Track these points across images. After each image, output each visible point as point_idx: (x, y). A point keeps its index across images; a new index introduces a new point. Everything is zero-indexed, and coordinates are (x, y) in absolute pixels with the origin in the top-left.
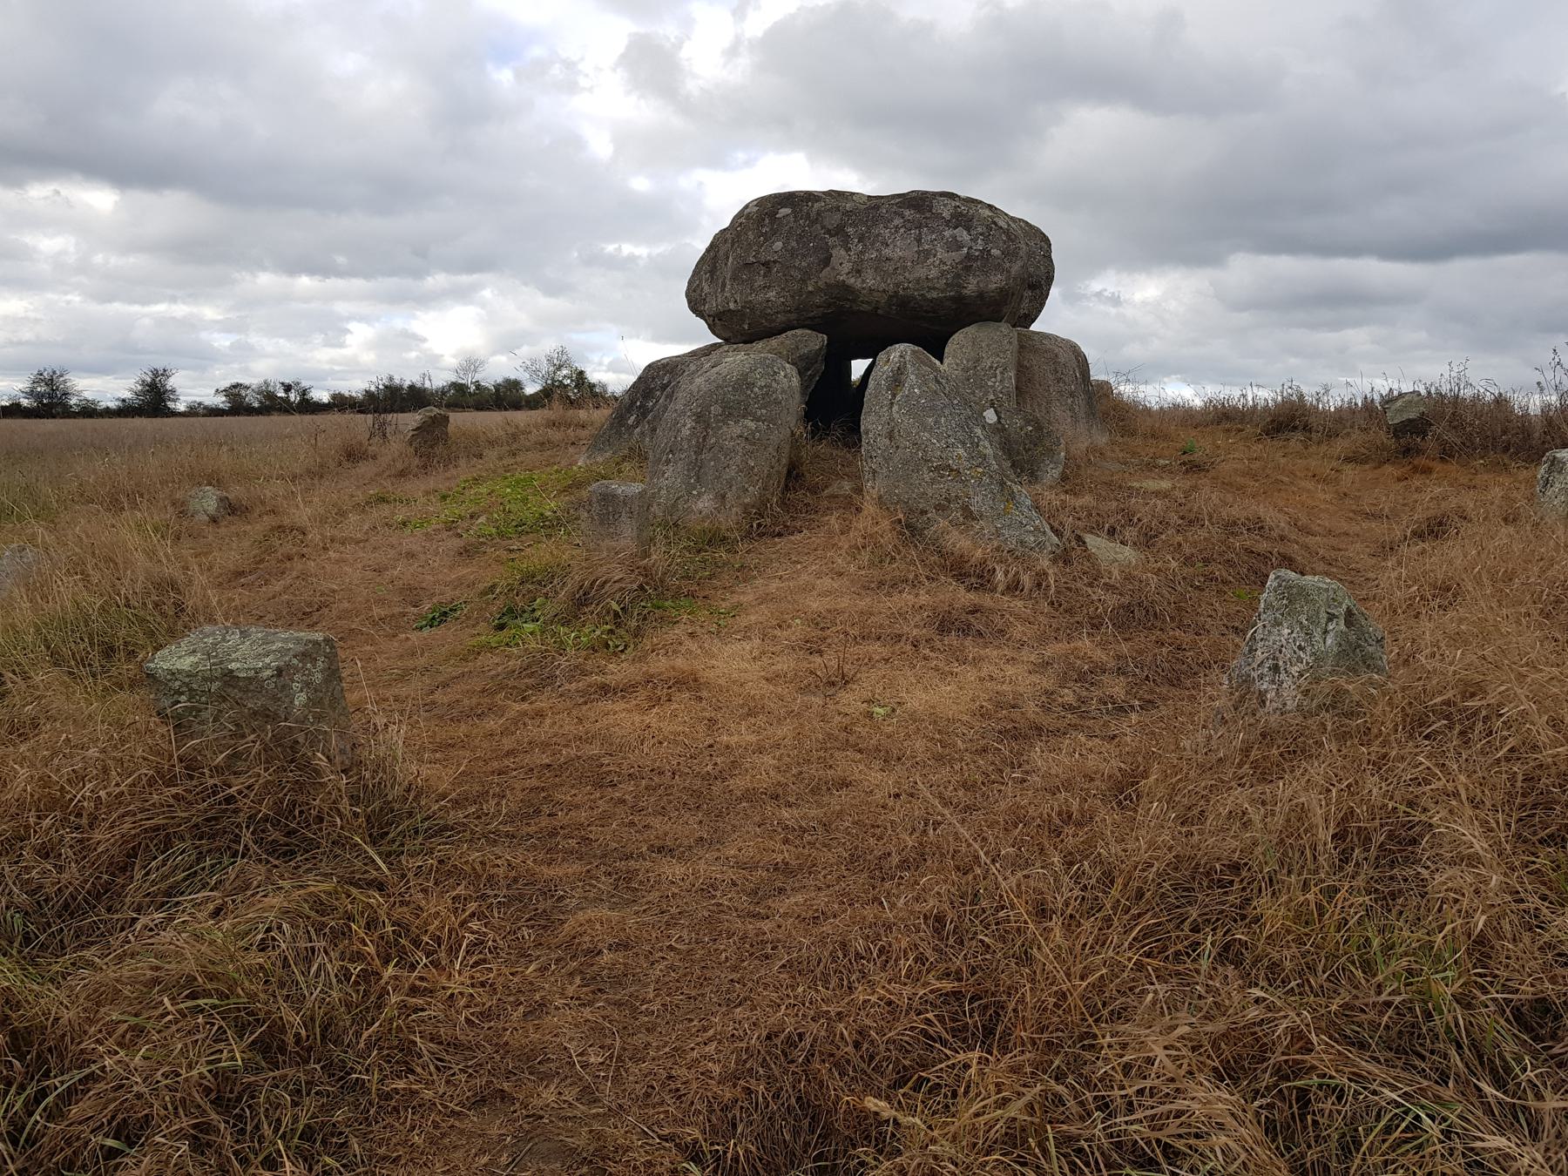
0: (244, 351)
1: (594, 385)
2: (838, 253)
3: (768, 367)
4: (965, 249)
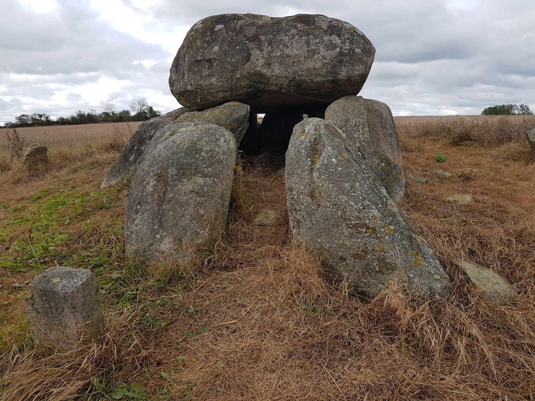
0: (17, 102)
1: (156, 112)
2: (255, 53)
3: (211, 135)
4: (338, 49)
